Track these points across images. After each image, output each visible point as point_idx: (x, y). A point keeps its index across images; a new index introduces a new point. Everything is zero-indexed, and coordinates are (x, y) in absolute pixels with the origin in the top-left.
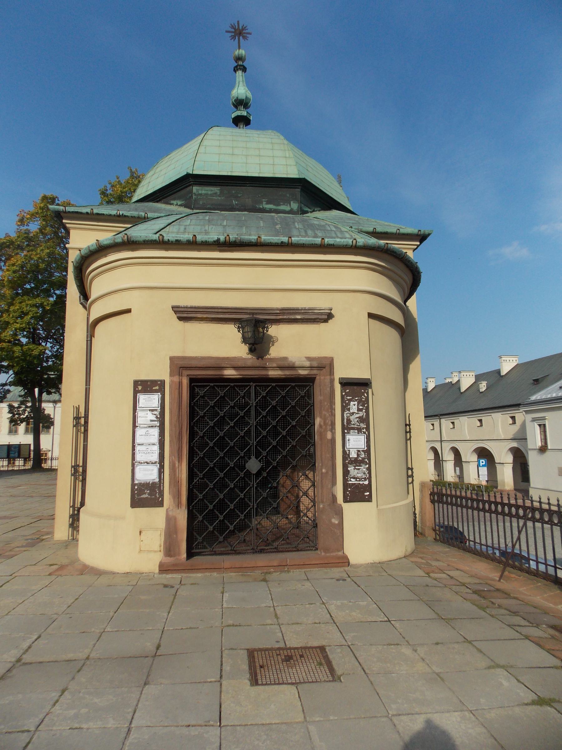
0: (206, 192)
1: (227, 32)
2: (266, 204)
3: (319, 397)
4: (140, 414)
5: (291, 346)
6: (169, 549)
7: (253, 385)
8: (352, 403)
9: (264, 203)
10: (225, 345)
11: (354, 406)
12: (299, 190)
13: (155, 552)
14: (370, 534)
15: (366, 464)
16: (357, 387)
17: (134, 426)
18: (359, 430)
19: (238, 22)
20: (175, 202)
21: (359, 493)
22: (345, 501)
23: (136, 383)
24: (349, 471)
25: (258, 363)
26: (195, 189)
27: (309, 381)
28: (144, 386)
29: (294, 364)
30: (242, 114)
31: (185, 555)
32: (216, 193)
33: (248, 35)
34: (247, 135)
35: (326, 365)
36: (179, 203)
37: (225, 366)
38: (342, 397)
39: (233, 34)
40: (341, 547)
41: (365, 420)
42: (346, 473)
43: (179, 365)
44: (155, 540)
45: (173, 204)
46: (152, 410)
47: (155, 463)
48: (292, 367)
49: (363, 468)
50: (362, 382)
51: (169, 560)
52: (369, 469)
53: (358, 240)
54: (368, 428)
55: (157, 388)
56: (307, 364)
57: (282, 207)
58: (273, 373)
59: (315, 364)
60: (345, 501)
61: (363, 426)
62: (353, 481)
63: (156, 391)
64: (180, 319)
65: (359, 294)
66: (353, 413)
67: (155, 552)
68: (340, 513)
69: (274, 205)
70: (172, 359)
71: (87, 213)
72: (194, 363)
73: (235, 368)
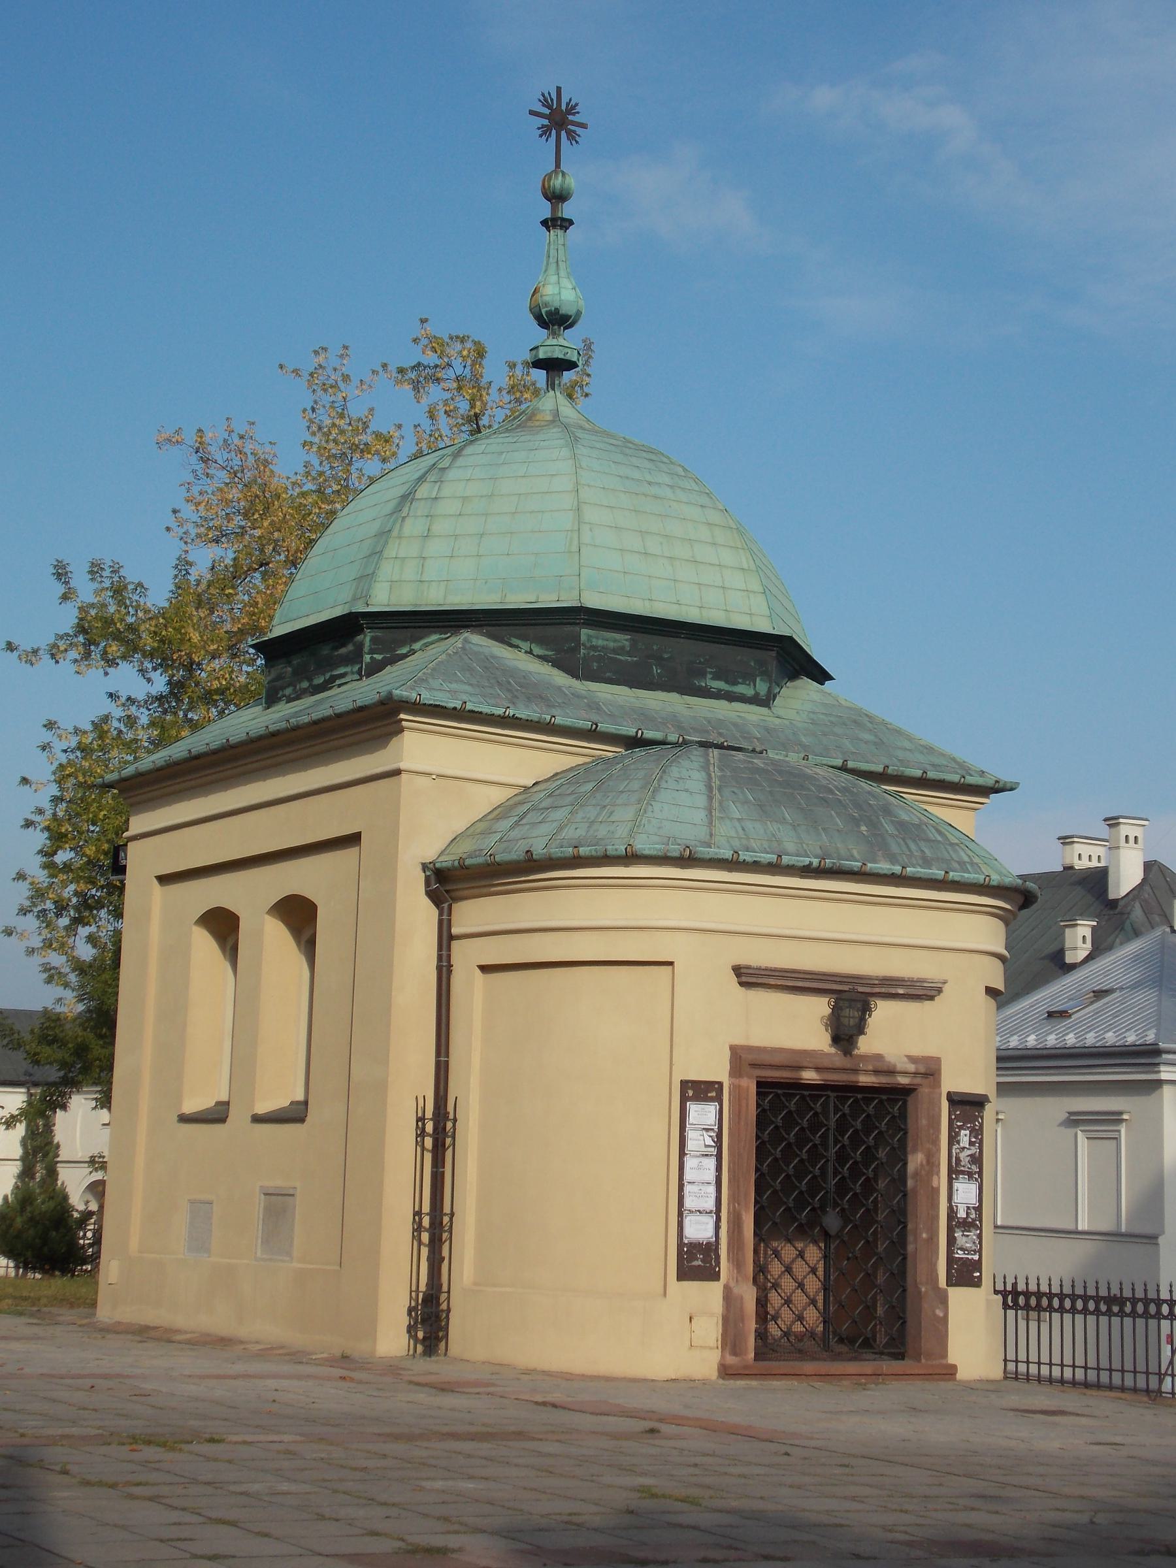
0: (605, 643)
1: (532, 113)
2: (712, 679)
3: (918, 1120)
4: (691, 1135)
5: (891, 1035)
6: (730, 1340)
7: (832, 1095)
8: (963, 1132)
9: (709, 676)
10: (797, 1028)
11: (964, 1137)
12: (774, 654)
13: (711, 1348)
14: (972, 1333)
15: (977, 1228)
16: (968, 1106)
17: (682, 1153)
18: (970, 1175)
19: (559, 89)
20: (525, 645)
21: (965, 1273)
22: (949, 1283)
23: (684, 1084)
24: (955, 1238)
25: (839, 1060)
26: (585, 633)
27: (906, 1092)
28: (698, 1090)
29: (895, 1066)
30: (568, 357)
31: (752, 1355)
32: (623, 648)
33: (579, 130)
34: (654, 490)
35: (930, 1070)
36: (537, 650)
37: (805, 1064)
38: (950, 1121)
39: (546, 122)
40: (945, 1355)
41: (977, 1160)
42: (951, 1241)
43: (742, 1059)
44: (710, 1330)
45: (517, 647)
46: (707, 1130)
47: (711, 1212)
48: (892, 1072)
49: (973, 1234)
50: (971, 1099)
51: (731, 1360)
52: (980, 1236)
53: (993, 877)
54: (980, 1173)
55: (714, 1094)
56: (911, 1068)
57: (741, 689)
58: (865, 1080)
59: (922, 1069)
60: (949, 1283)
61: (975, 1168)
62: (960, 1254)
63: (712, 1100)
64: (741, 984)
65: (976, 956)
66: (964, 1148)
67: (711, 1348)
68: (944, 1300)
69: (727, 682)
70: (734, 1049)
71: (455, 708)
72: (767, 1059)
73: (818, 1069)
